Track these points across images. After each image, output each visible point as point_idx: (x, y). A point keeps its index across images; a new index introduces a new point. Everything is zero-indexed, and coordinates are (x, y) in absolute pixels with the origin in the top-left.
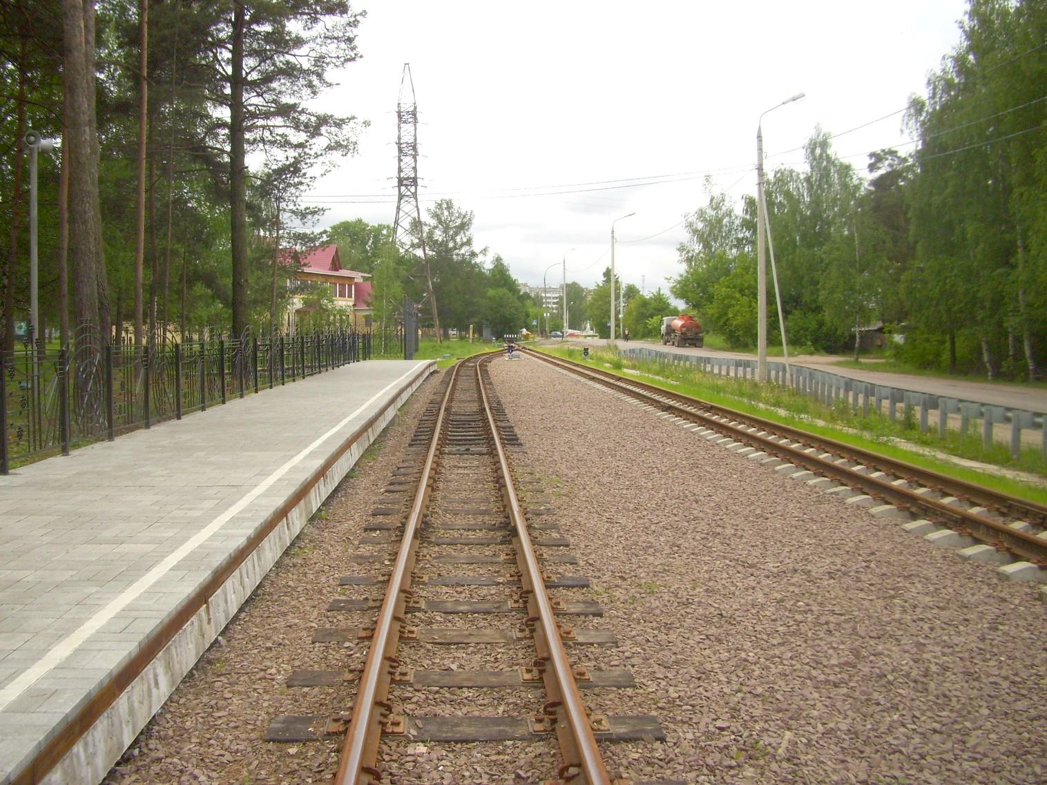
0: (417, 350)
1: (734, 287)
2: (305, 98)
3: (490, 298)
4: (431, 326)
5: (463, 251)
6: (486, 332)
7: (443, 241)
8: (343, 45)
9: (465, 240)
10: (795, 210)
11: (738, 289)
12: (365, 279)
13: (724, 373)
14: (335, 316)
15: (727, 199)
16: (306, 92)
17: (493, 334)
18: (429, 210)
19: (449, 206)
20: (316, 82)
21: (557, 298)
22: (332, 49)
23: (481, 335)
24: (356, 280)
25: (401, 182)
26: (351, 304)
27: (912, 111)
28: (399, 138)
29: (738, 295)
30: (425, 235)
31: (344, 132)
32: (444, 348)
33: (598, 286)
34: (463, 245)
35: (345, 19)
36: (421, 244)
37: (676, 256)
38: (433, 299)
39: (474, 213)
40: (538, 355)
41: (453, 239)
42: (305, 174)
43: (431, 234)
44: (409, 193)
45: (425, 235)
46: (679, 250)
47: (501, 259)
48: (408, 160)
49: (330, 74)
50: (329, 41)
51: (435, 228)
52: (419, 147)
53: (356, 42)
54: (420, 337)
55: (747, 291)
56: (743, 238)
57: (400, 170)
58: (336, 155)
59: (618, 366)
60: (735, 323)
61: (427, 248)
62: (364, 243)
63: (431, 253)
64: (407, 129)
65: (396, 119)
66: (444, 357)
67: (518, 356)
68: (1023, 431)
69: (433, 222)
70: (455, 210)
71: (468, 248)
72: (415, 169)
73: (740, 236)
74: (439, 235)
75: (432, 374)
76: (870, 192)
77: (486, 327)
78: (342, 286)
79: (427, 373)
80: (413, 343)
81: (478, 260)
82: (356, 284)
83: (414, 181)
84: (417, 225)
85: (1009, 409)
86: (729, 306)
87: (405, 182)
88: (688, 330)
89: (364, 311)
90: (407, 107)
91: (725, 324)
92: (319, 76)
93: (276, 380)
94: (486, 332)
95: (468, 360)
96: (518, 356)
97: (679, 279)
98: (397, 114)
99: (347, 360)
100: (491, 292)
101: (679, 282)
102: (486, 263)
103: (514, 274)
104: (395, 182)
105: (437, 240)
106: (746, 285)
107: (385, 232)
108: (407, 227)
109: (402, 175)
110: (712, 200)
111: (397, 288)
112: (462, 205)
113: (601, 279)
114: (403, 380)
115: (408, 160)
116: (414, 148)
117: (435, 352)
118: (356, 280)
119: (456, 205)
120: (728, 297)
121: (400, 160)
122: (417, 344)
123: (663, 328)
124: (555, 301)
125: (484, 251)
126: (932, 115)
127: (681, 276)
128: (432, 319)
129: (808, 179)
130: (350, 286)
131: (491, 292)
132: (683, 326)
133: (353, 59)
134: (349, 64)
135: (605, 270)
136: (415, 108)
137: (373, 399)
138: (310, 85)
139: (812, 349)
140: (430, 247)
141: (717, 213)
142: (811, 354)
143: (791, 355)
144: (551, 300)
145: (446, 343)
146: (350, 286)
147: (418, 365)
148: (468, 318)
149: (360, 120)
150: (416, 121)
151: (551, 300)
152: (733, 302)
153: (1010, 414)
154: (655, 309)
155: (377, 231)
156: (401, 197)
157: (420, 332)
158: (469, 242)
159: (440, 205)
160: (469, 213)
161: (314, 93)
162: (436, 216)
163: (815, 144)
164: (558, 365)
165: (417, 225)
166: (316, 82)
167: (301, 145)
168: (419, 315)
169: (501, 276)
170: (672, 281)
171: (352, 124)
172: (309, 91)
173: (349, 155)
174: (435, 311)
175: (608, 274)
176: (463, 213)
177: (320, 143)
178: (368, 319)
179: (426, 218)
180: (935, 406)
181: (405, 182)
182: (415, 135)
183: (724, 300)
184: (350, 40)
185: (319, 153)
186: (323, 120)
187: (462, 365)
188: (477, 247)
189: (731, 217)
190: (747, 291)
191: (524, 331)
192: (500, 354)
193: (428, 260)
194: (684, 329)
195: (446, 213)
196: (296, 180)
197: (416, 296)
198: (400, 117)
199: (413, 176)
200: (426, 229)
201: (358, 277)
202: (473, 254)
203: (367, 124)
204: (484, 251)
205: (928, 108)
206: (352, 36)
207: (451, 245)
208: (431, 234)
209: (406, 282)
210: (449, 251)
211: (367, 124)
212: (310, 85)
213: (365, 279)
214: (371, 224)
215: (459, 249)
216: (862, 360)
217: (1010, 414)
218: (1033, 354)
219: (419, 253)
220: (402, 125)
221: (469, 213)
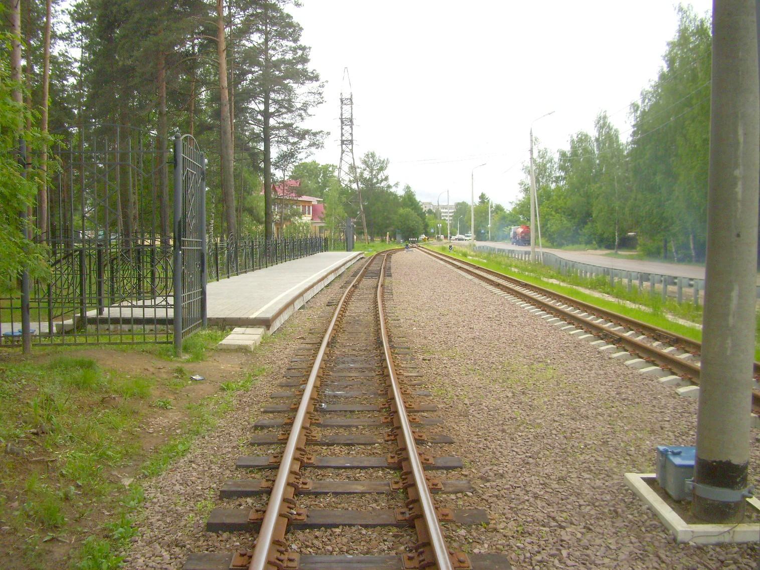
0: (353, 248)
1: (552, 208)
2: (298, 121)
3: (400, 215)
4: (362, 233)
5: (382, 185)
6: (399, 237)
7: (370, 178)
8: (317, 96)
9: (384, 177)
10: (589, 161)
11: (554, 209)
12: (319, 201)
13: (520, 258)
14: (303, 228)
15: (548, 150)
16: (298, 118)
17: (402, 239)
18: (361, 159)
19: (373, 156)
20: (304, 114)
21: (452, 212)
22: (311, 98)
23: (395, 239)
24: (313, 203)
25: (343, 142)
26: (310, 218)
27: (632, 110)
28: (342, 115)
29: (553, 213)
30: (358, 175)
31: (317, 138)
32: (370, 246)
33: (476, 205)
34: (382, 181)
35: (318, 83)
36: (356, 180)
37: (518, 188)
38: (363, 216)
39: (389, 159)
40: (428, 251)
41: (376, 176)
42: (297, 157)
43: (362, 173)
44: (348, 150)
45: (358, 175)
46: (519, 184)
47: (410, 188)
48: (347, 128)
49: (310, 110)
50: (310, 94)
51: (365, 170)
52: (354, 121)
53: (323, 95)
54: (355, 240)
55: (560, 210)
56: (559, 177)
57: (342, 135)
58: (313, 149)
59: (465, 255)
60: (552, 230)
61: (359, 183)
62: (317, 176)
63: (362, 186)
64: (347, 115)
65: (340, 103)
66: (368, 251)
67: (412, 251)
68: (668, 286)
69: (363, 166)
70: (377, 159)
71: (386, 182)
72: (351, 134)
73: (558, 175)
74: (367, 175)
75: (361, 258)
76: (633, 149)
77: (399, 233)
78: (304, 207)
79: (358, 258)
80: (351, 244)
81: (393, 190)
82: (313, 206)
83: (351, 142)
84: (353, 168)
85: (691, 279)
86: (548, 220)
87: (345, 142)
88: (525, 235)
89: (319, 224)
90: (346, 95)
91: (546, 230)
92: (305, 111)
93: (263, 265)
94: (399, 237)
95: (382, 252)
96: (412, 251)
97: (518, 202)
98: (340, 121)
99: (318, 251)
100: (401, 211)
101: (518, 205)
102: (400, 192)
103: (418, 198)
104: (340, 143)
105: (366, 178)
106: (559, 206)
107: (330, 169)
108: (347, 170)
109: (344, 138)
110: (539, 152)
111: (340, 210)
112: (381, 155)
113: (477, 201)
114: (347, 258)
115: (347, 128)
116: (351, 121)
117: (365, 248)
118: (313, 203)
119: (377, 155)
120: (548, 214)
121: (342, 129)
122: (353, 245)
123: (512, 233)
124: (451, 214)
125: (396, 185)
126: (644, 113)
127: (520, 201)
128: (363, 228)
129: (597, 140)
130: (309, 207)
131: (401, 211)
132: (522, 232)
133: (322, 103)
134: (319, 105)
135: (480, 195)
136: (352, 95)
137: (332, 266)
138: (300, 115)
139: (596, 246)
140: (361, 182)
141: (543, 160)
142: (596, 249)
143: (544, 246)
144: (447, 216)
145: (371, 244)
146: (309, 207)
147: (353, 254)
148: (386, 227)
149: (326, 132)
150: (352, 103)
151: (447, 216)
152: (551, 217)
153: (692, 282)
154: (510, 221)
155: (326, 169)
156: (343, 152)
157: (355, 237)
158: (386, 179)
159: (368, 155)
160: (386, 160)
161: (302, 119)
162: (365, 162)
163: (600, 118)
164: (430, 254)
165: (353, 168)
166: (304, 114)
167: (294, 144)
168: (355, 226)
169: (410, 200)
170: (514, 204)
171: (321, 134)
172: (300, 118)
173: (320, 148)
174: (365, 224)
175: (482, 197)
176: (382, 160)
177: (305, 143)
178: (321, 228)
179: (358, 163)
180: (648, 280)
181: (345, 142)
182: (352, 113)
183: (545, 216)
184: (320, 94)
185: (304, 147)
186: (307, 132)
187: (378, 254)
188: (391, 182)
189: (551, 163)
190: (560, 210)
191: (423, 236)
192: (402, 250)
193: (361, 191)
194: (523, 234)
195: (371, 160)
196: (292, 160)
197: (353, 214)
198: (342, 102)
199: (350, 139)
200: (358, 171)
201: (314, 200)
202: (389, 187)
203: (328, 133)
204: (396, 185)
205: (641, 109)
206: (321, 92)
207: (375, 181)
208: (362, 173)
209: (346, 205)
210: (372, 185)
211: (328, 133)
212: (300, 115)
213: (319, 201)
214: (321, 164)
215: (380, 183)
216: (619, 252)
217: (692, 282)
218: (694, 248)
219: (354, 186)
220: (344, 106)
221: (386, 160)
